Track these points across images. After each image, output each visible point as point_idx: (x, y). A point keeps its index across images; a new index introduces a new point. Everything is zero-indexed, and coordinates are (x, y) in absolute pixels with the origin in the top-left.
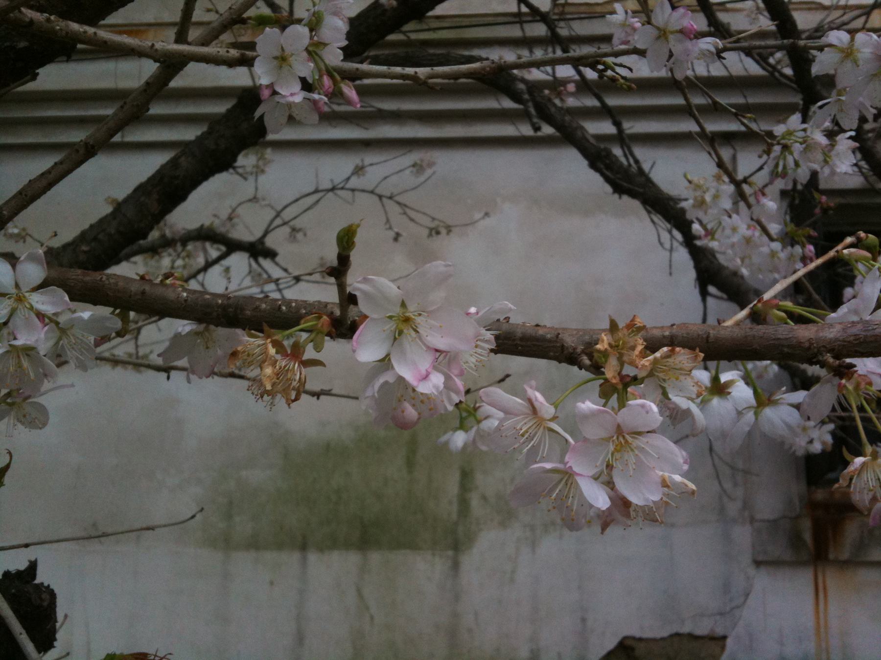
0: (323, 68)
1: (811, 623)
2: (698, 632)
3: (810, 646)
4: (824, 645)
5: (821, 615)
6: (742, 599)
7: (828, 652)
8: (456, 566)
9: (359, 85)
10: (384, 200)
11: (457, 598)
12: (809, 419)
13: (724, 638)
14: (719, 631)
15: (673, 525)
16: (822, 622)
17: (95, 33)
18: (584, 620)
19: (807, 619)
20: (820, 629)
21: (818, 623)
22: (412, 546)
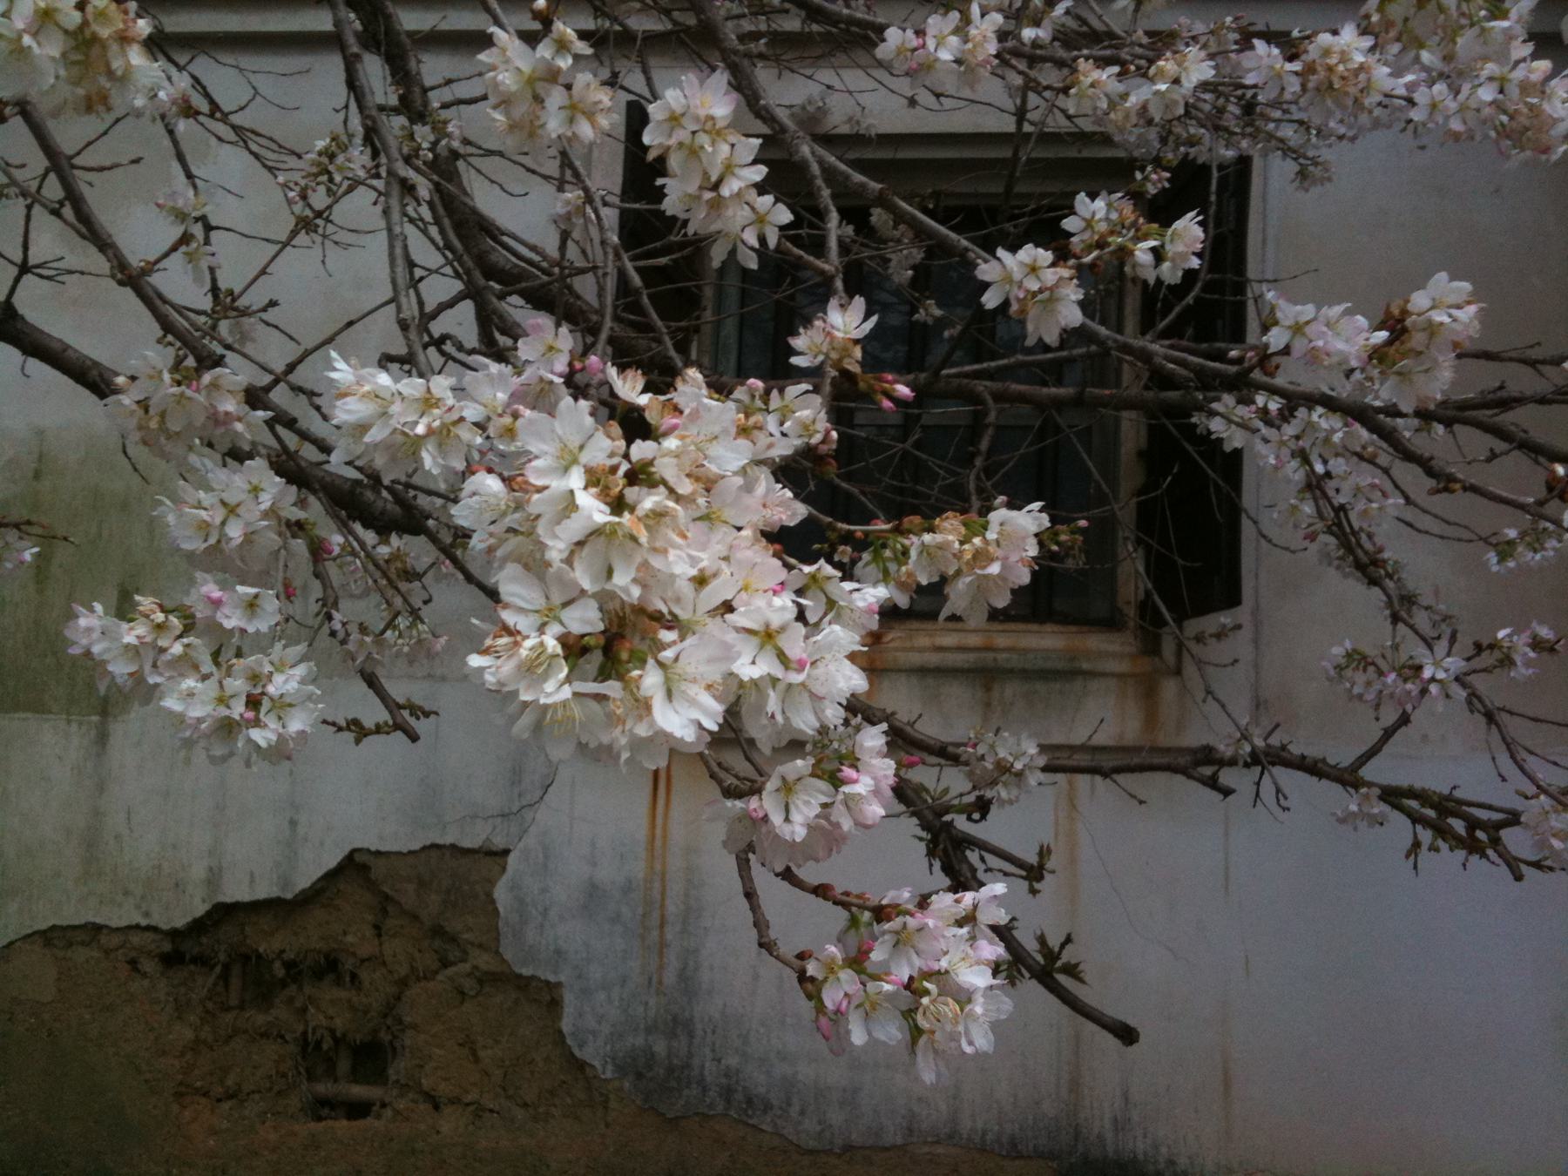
0: (1490, 852)
1: (642, 834)
2: (467, 843)
3: (638, 869)
4: (658, 867)
5: (659, 821)
6: (538, 793)
7: (663, 880)
8: (102, 739)
9: (645, 268)
10: (392, 307)
11: (101, 788)
12: (739, 529)
13: (506, 852)
14: (499, 842)
15: (443, 679)
16: (659, 832)
17: (995, 660)
18: (293, 823)
19: (637, 825)
20: (655, 843)
21: (653, 837)
22: (38, 708)
